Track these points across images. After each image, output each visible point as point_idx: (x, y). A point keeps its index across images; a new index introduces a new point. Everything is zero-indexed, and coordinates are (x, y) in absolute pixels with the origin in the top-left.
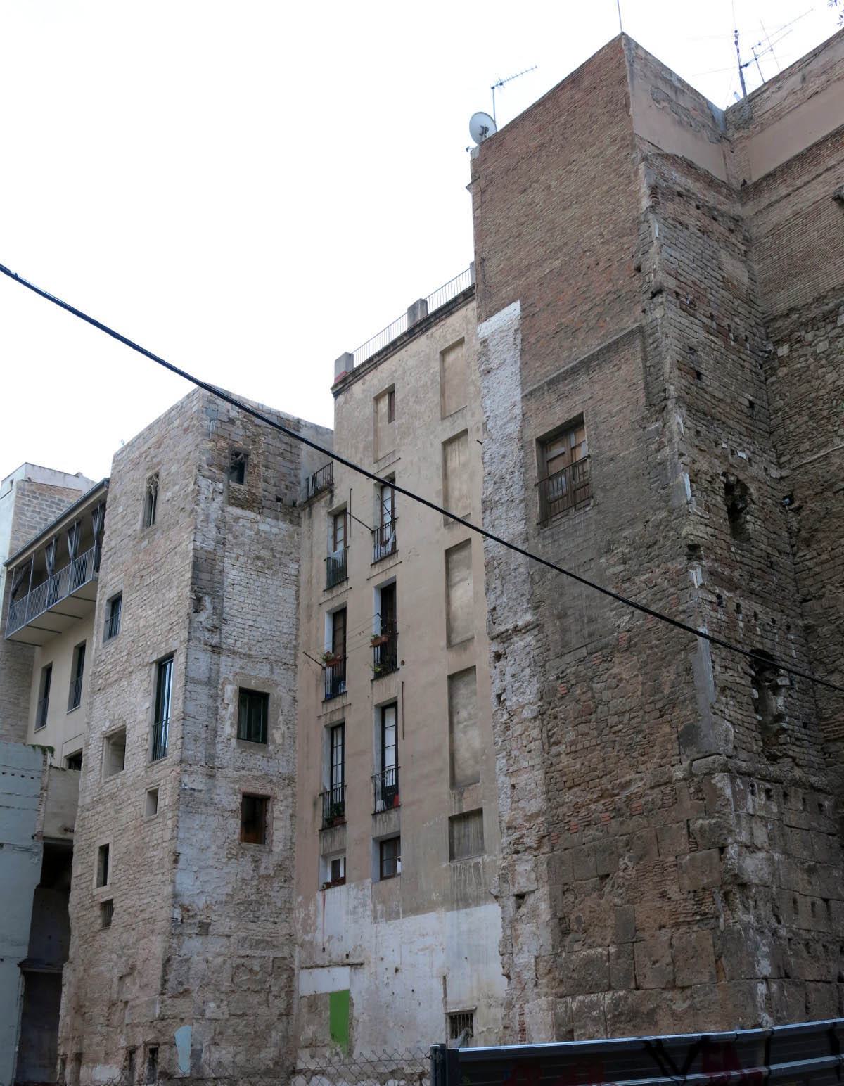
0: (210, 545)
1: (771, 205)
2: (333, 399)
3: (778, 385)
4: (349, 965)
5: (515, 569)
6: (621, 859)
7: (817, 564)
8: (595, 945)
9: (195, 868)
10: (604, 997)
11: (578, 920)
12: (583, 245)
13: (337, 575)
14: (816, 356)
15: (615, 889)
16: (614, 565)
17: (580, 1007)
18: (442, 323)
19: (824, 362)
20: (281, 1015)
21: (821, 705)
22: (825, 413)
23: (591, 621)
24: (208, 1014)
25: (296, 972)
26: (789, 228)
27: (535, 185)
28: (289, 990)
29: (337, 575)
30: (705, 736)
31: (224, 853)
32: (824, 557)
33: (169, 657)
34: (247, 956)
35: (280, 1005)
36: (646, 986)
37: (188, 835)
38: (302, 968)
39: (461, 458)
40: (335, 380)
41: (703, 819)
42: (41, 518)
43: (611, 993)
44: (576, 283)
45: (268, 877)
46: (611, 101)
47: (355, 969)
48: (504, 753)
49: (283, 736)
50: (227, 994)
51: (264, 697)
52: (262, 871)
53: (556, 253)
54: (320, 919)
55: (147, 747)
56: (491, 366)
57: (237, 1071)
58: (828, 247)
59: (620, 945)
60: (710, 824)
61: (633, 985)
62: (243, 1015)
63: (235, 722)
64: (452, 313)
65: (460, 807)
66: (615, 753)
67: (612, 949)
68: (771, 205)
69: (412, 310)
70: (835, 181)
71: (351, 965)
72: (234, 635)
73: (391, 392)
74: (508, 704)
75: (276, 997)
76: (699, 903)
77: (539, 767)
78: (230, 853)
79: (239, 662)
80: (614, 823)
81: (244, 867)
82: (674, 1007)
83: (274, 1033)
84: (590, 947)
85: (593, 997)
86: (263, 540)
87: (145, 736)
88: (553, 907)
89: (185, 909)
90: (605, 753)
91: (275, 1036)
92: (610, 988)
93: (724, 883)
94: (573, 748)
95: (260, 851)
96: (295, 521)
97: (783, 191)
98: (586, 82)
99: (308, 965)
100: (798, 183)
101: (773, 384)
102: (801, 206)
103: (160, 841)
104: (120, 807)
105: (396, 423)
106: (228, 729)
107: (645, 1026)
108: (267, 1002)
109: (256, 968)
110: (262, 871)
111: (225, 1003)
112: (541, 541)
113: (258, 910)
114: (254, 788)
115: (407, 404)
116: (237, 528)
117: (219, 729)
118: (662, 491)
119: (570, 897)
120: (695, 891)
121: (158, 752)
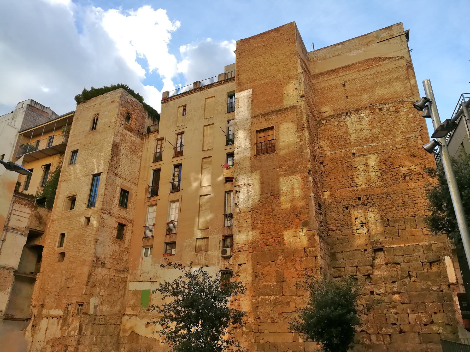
0: (118, 141)
1: (322, 81)
2: (76, 105)
3: (321, 131)
4: (151, 281)
5: (245, 167)
6: (279, 257)
7: (329, 182)
8: (268, 281)
9: (102, 245)
10: (271, 298)
11: (262, 274)
12: (276, 78)
13: (158, 158)
14: (334, 126)
15: (276, 265)
16: (282, 172)
17: (261, 300)
18: (207, 90)
19: (336, 127)
20: (122, 296)
21: (328, 221)
22: (336, 141)
23: (272, 186)
24: (101, 294)
25: (128, 282)
26: (327, 89)
27: (260, 57)
28: (125, 287)
29: (158, 158)
30: (312, 224)
31: (111, 241)
32: (332, 180)
33: (99, 174)
34: (114, 276)
35: (121, 293)
36: (286, 294)
37: (101, 234)
38: (131, 281)
39: (210, 132)
40: (163, 98)
41: (310, 248)
42: (33, 119)
43: (274, 296)
44: (273, 88)
45: (122, 251)
46: (289, 39)
48: (237, 221)
49: (132, 206)
50: (107, 287)
51: (128, 192)
52: (121, 249)
53: (266, 78)
54: (140, 267)
55: (86, 203)
56: (239, 106)
57: (107, 314)
58: (339, 97)
59: (278, 282)
60: (313, 250)
61: (282, 294)
62: (111, 295)
63: (119, 199)
64: (211, 88)
65: (39, 244)
66: (279, 225)
67: (275, 283)
68: (322, 81)
69: (195, 83)
70: (342, 80)
72: (122, 171)
73: (185, 106)
74: (239, 206)
75: (121, 290)
76: (307, 272)
77: (250, 226)
78: (113, 242)
79: (122, 180)
80: (277, 246)
81: (116, 247)
82: (296, 302)
83: (119, 302)
84: (266, 282)
85: (267, 297)
86: (133, 142)
87: (86, 199)
88: (253, 269)
89: (98, 258)
90: (275, 225)
91: (119, 302)
92: (273, 294)
93: (316, 267)
94: (263, 222)
95: (122, 242)
96: (142, 139)
97: (326, 79)
98: (281, 32)
99: (133, 280)
100: (331, 77)
101: (319, 130)
102: (331, 84)
103: (90, 234)
104: (71, 221)
105: (186, 116)
106: (117, 201)
107: (286, 306)
108: (118, 291)
109: (117, 280)
110: (121, 249)
111: (106, 290)
112: (256, 160)
113: (119, 261)
114: (122, 221)
115: (191, 112)
116: (126, 137)
117: (114, 201)
118: (301, 153)
119: (259, 266)
120: (306, 269)
121: (91, 204)
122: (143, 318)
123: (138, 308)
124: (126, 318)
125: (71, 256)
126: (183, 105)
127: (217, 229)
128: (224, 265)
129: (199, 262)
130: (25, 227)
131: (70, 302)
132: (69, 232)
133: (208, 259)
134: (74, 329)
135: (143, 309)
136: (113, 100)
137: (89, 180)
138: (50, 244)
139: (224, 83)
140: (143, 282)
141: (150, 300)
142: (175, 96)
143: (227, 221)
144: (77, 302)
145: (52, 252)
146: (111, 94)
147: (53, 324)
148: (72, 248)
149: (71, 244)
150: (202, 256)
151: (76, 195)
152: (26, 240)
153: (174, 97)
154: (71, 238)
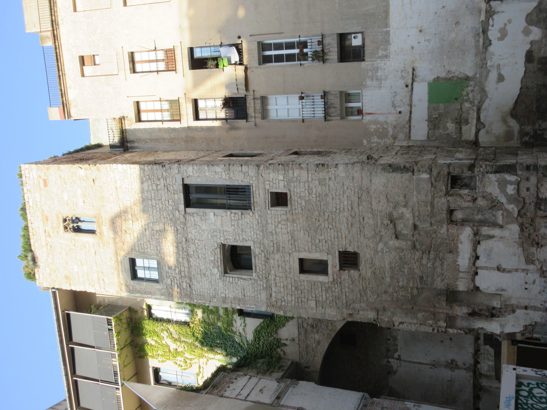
18: (58, 11)
38: (410, 137)
54: (381, 118)
55: (240, 213)
104: (275, 245)
122: (485, 92)
123: (464, 109)
124: (483, 138)
130: (278, 384)
131: (444, 215)
132: (297, 249)
134: (502, 185)
136: (42, 182)
137: (195, 215)
138: (319, 301)
140: (413, 105)
143: (316, 115)
144: (447, 194)
145: (337, 290)
146: (30, 191)
148: (332, 231)
151: (224, 245)
152: (305, 382)
154: (310, 239)
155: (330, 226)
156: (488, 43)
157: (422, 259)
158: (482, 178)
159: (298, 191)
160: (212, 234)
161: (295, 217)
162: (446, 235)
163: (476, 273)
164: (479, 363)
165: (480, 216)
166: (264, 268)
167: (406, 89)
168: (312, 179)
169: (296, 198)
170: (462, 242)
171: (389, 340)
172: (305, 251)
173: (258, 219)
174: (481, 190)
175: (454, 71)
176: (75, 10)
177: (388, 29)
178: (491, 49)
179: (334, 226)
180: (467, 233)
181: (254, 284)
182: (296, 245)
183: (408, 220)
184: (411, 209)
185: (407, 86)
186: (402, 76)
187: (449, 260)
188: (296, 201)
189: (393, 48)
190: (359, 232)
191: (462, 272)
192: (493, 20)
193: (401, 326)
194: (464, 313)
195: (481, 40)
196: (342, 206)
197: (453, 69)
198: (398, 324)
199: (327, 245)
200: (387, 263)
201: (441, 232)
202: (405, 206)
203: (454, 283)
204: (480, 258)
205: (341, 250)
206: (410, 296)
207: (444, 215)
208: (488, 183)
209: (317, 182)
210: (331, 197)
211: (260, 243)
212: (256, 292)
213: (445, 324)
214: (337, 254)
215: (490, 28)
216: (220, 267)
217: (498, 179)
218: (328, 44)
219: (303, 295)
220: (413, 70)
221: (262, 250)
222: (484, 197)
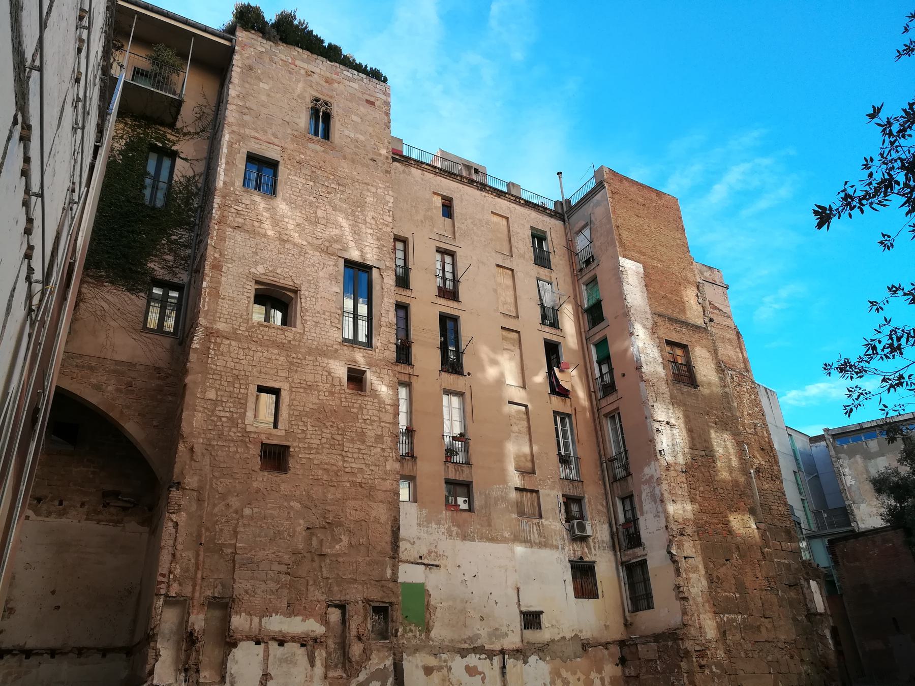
4: (423, 564)
47: (430, 569)
64: (499, 197)
71: (427, 565)
122: (415, 653)
125: (315, 462)
126: (445, 194)
127: (551, 480)
128: (574, 550)
129: (529, 538)
133: (544, 533)
135: (411, 631)
139: (522, 205)
141: (428, 609)
142: (427, 164)
144: (367, 601)
145: (232, 434)
147: (289, 661)
149: (310, 427)
150: (533, 527)
153: (423, 166)
154: (308, 410)
155: (324, 440)
156: (463, 653)
157: (279, 564)
158: (387, 647)
159: (369, 407)
160: (312, 282)
161: (336, 395)
162: (312, 599)
163: (258, 643)
164: (27, 657)
165: (333, 646)
166: (265, 337)
167: (417, 556)
168: (382, 427)
169: (359, 402)
170: (305, 622)
171: (61, 504)
172: (292, 400)
173: (332, 347)
174: (373, 646)
175: (436, 614)
176: (434, 193)
177: (477, 540)
178: (458, 658)
179: (325, 445)
180: (314, 627)
181: (241, 317)
182: (299, 390)
183: (332, 547)
184: (346, 552)
185: (421, 557)
186: (431, 553)
187: (278, 602)
188: (356, 401)
189: (459, 543)
190: (316, 477)
191: (260, 621)
192: (485, 659)
193: (171, 524)
194: (193, 624)
195: (466, 646)
196: (349, 460)
197: (439, 613)
198: (175, 520)
199: (300, 431)
200: (273, 512)
201: (316, 593)
202: (351, 545)
203: (242, 609)
204: (282, 648)
205: (291, 449)
206: (220, 542)
207: (339, 596)
208: (382, 656)
209: (380, 433)
210: (361, 447)
211: (300, 341)
212: (229, 317)
213: (174, 595)
214: (287, 444)
215: (478, 656)
216: (267, 277)
217: (387, 669)
218: (462, 470)
219: (226, 384)
220: (437, 566)
221: (290, 341)
222: (364, 650)
